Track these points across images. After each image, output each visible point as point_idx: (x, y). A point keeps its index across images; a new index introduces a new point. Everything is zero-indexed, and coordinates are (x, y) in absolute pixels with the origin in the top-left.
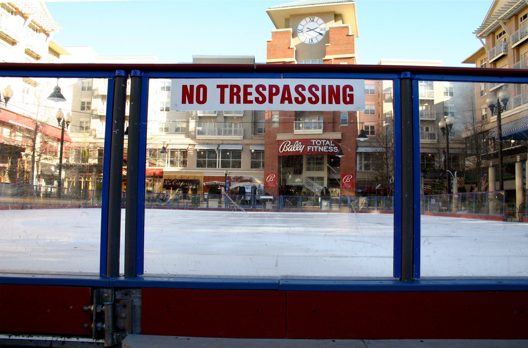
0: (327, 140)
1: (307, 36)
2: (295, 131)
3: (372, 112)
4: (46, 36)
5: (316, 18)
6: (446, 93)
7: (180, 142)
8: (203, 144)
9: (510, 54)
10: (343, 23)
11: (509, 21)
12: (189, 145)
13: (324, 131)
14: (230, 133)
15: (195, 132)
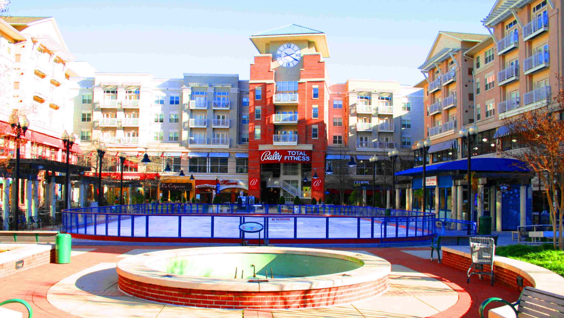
0: (300, 151)
1: (284, 61)
2: (274, 143)
3: (340, 124)
4: (49, 55)
5: (292, 45)
6: (404, 108)
7: (175, 150)
8: (195, 152)
9: (521, 47)
10: (317, 51)
12: (183, 153)
13: (298, 143)
14: (218, 142)
15: (187, 141)
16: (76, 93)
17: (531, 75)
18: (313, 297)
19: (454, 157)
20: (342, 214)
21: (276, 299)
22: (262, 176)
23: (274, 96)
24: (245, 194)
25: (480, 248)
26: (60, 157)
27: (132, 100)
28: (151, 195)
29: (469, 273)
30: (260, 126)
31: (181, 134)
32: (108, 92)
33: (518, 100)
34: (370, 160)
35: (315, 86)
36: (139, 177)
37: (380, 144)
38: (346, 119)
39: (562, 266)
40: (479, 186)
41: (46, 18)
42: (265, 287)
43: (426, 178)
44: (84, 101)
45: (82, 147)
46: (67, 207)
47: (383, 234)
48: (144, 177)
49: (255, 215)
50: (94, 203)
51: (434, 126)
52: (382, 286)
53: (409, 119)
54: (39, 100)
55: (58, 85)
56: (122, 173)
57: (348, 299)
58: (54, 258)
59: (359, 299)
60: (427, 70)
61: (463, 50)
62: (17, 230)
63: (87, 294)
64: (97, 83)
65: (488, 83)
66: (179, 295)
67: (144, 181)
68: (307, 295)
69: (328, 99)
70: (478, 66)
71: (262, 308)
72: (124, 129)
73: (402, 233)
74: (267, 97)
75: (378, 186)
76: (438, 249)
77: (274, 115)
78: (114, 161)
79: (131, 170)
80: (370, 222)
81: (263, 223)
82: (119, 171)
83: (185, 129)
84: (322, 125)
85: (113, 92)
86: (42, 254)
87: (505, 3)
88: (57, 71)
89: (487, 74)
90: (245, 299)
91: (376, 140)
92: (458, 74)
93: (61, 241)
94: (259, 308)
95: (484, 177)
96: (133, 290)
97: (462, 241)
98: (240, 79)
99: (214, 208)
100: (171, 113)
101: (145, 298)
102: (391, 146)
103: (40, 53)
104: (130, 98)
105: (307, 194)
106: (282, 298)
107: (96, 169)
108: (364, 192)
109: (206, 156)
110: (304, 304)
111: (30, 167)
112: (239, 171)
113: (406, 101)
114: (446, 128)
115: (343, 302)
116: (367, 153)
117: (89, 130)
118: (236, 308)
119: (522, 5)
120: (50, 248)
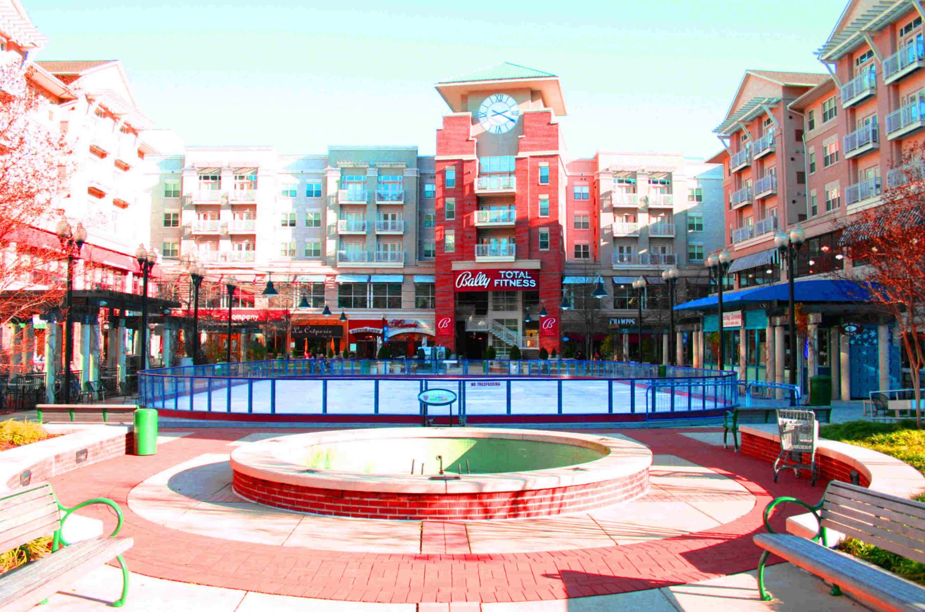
0: (520, 270)
3: (585, 225)
5: (505, 97)
7: (315, 272)
10: (545, 106)
11: (878, 34)
12: (328, 275)
13: (517, 258)
15: (335, 256)
16: (155, 181)
17: (899, 141)
18: (527, 502)
19: (775, 277)
20: (590, 375)
21: (471, 504)
22: (457, 313)
23: (476, 180)
24: (431, 343)
25: (796, 427)
26: (129, 285)
27: (245, 190)
28: (276, 345)
29: (778, 466)
30: (453, 231)
31: (324, 245)
32: (206, 178)
33: (878, 182)
34: (634, 284)
35: (544, 164)
36: (257, 317)
37: (653, 257)
38: (596, 217)
39: (921, 455)
40: (809, 327)
41: (108, 61)
42: (456, 487)
43: (724, 314)
44: (167, 194)
45: (165, 268)
46: (143, 367)
47: (650, 407)
48: (266, 317)
49: (445, 377)
50: (187, 361)
51: (741, 225)
52: (637, 486)
53: (700, 215)
54: (97, 193)
55: (126, 168)
56: (230, 310)
57: (582, 506)
58: (132, 445)
59: (600, 506)
60: (728, 135)
61: (786, 100)
62: (68, 403)
63: (186, 499)
64: (188, 164)
65: (828, 154)
66: (325, 500)
67: (264, 323)
68: (519, 499)
69: (566, 184)
70: (811, 126)
71: (450, 518)
72: (233, 237)
73: (681, 404)
74: (465, 183)
75: (649, 327)
76: (735, 430)
77: (476, 213)
78: (216, 291)
79: (244, 305)
80: (629, 387)
81: (457, 391)
82: (224, 307)
83: (332, 238)
84: (555, 227)
85: (214, 178)
86: (113, 440)
87: (853, 23)
88: (124, 147)
89: (827, 138)
90: (425, 505)
91: (645, 251)
92: (778, 140)
93: (142, 419)
94: (446, 518)
95: (818, 312)
96: (257, 494)
97: (768, 416)
98: (421, 154)
99: (380, 367)
100: (308, 210)
101: (274, 505)
102: (670, 260)
103: (99, 118)
104: (242, 188)
105: (530, 343)
106: (481, 504)
107: (189, 305)
108: (626, 338)
109: (364, 280)
110: (514, 512)
111: (87, 304)
112: (420, 305)
113: (694, 185)
114: (761, 230)
115: (574, 510)
116: (631, 273)
117: (177, 240)
118: (411, 518)
119: (881, 25)
120: (124, 431)
